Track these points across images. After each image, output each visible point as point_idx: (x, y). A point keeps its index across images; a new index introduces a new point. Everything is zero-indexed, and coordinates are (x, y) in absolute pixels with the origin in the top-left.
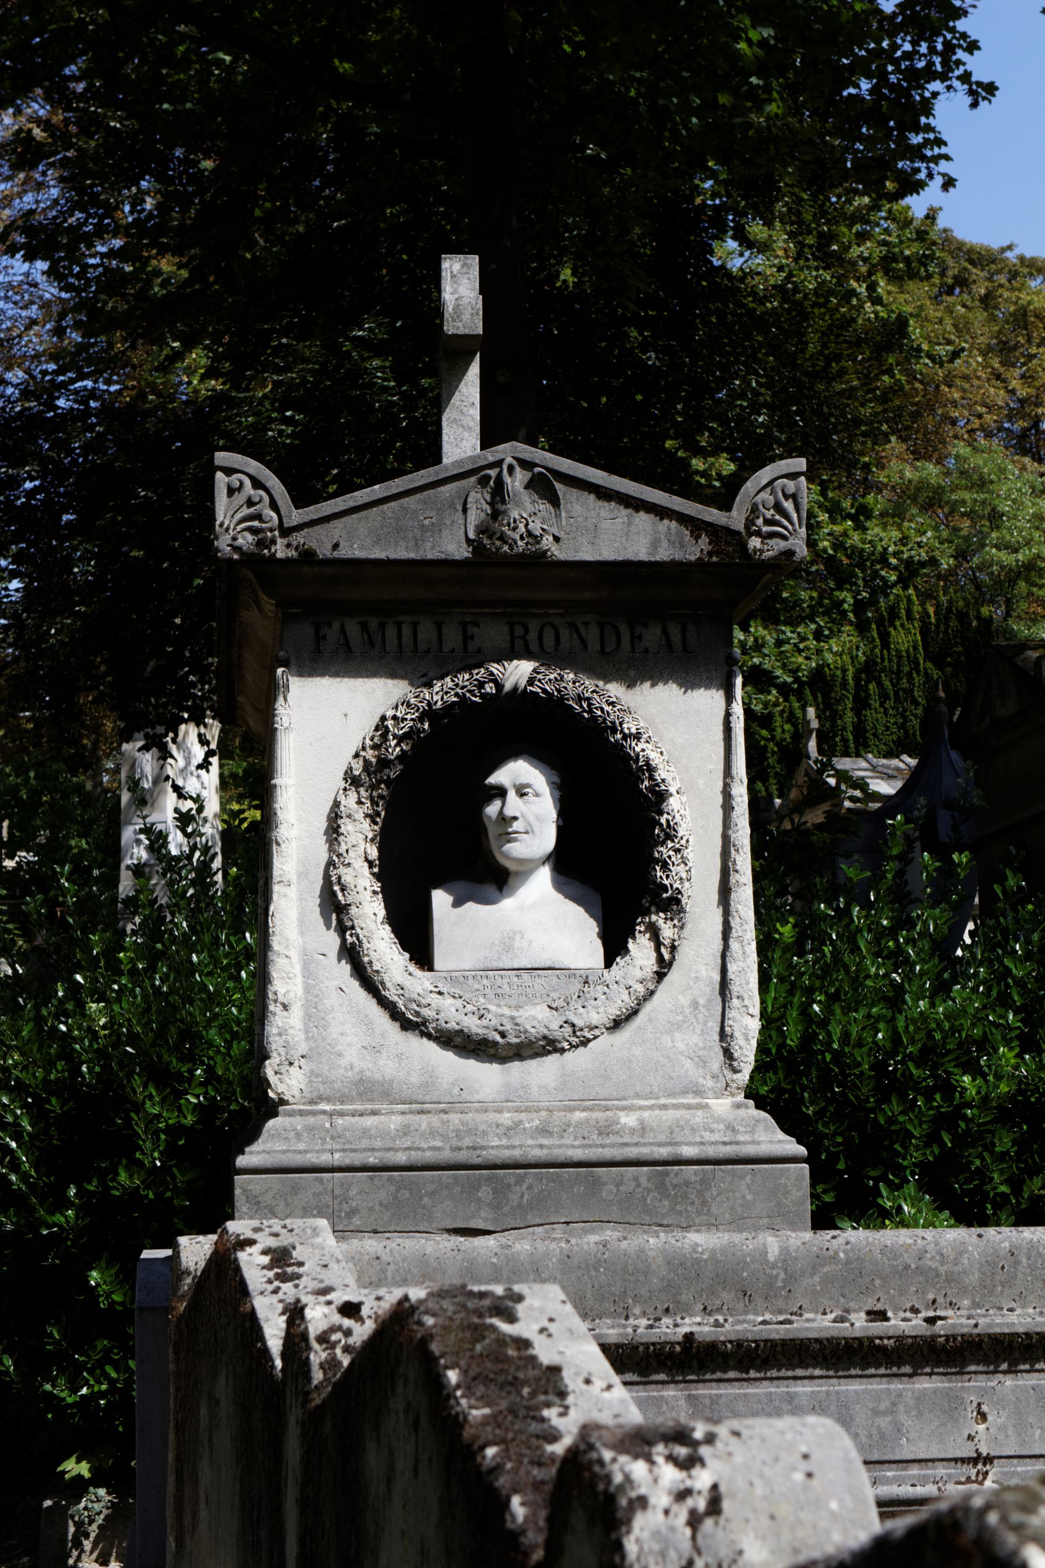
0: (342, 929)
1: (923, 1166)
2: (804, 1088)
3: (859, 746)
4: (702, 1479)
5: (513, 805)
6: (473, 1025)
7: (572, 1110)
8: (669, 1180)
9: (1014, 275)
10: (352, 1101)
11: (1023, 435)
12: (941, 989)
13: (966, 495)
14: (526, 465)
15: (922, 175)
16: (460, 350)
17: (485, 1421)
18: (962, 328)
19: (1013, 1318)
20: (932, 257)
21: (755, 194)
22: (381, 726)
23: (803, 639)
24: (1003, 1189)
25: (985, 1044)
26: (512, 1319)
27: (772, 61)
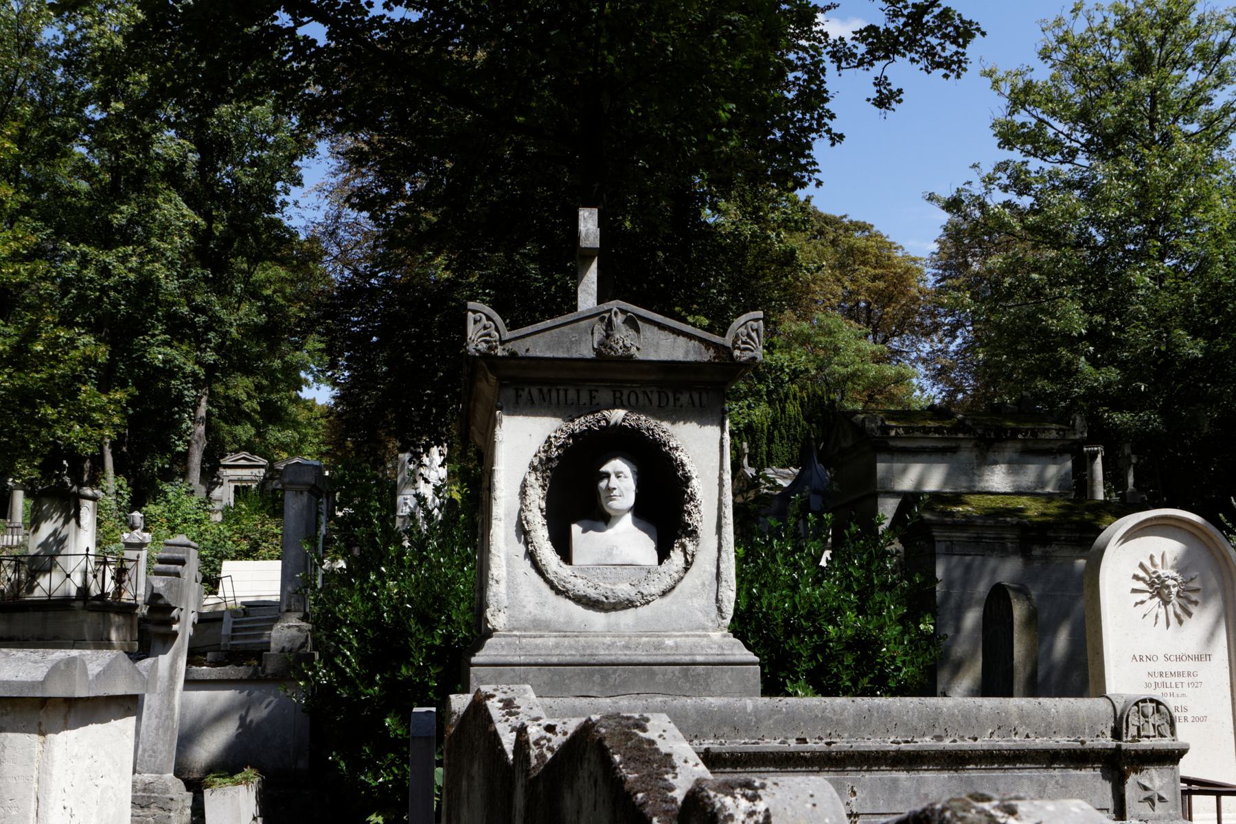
0: (527, 543)
1: (808, 672)
2: (748, 631)
3: (770, 461)
4: (761, 806)
5: (614, 482)
6: (592, 593)
7: (641, 636)
8: (691, 672)
9: (847, 230)
10: (530, 630)
11: (851, 309)
12: (817, 582)
13: (822, 339)
14: (623, 311)
15: (806, 179)
16: (588, 255)
17: (636, 780)
18: (821, 255)
19: (869, 743)
20: (808, 221)
21: (724, 185)
22: (548, 441)
23: (741, 408)
24: (848, 683)
25: (839, 610)
26: (645, 730)
27: (734, 122)
